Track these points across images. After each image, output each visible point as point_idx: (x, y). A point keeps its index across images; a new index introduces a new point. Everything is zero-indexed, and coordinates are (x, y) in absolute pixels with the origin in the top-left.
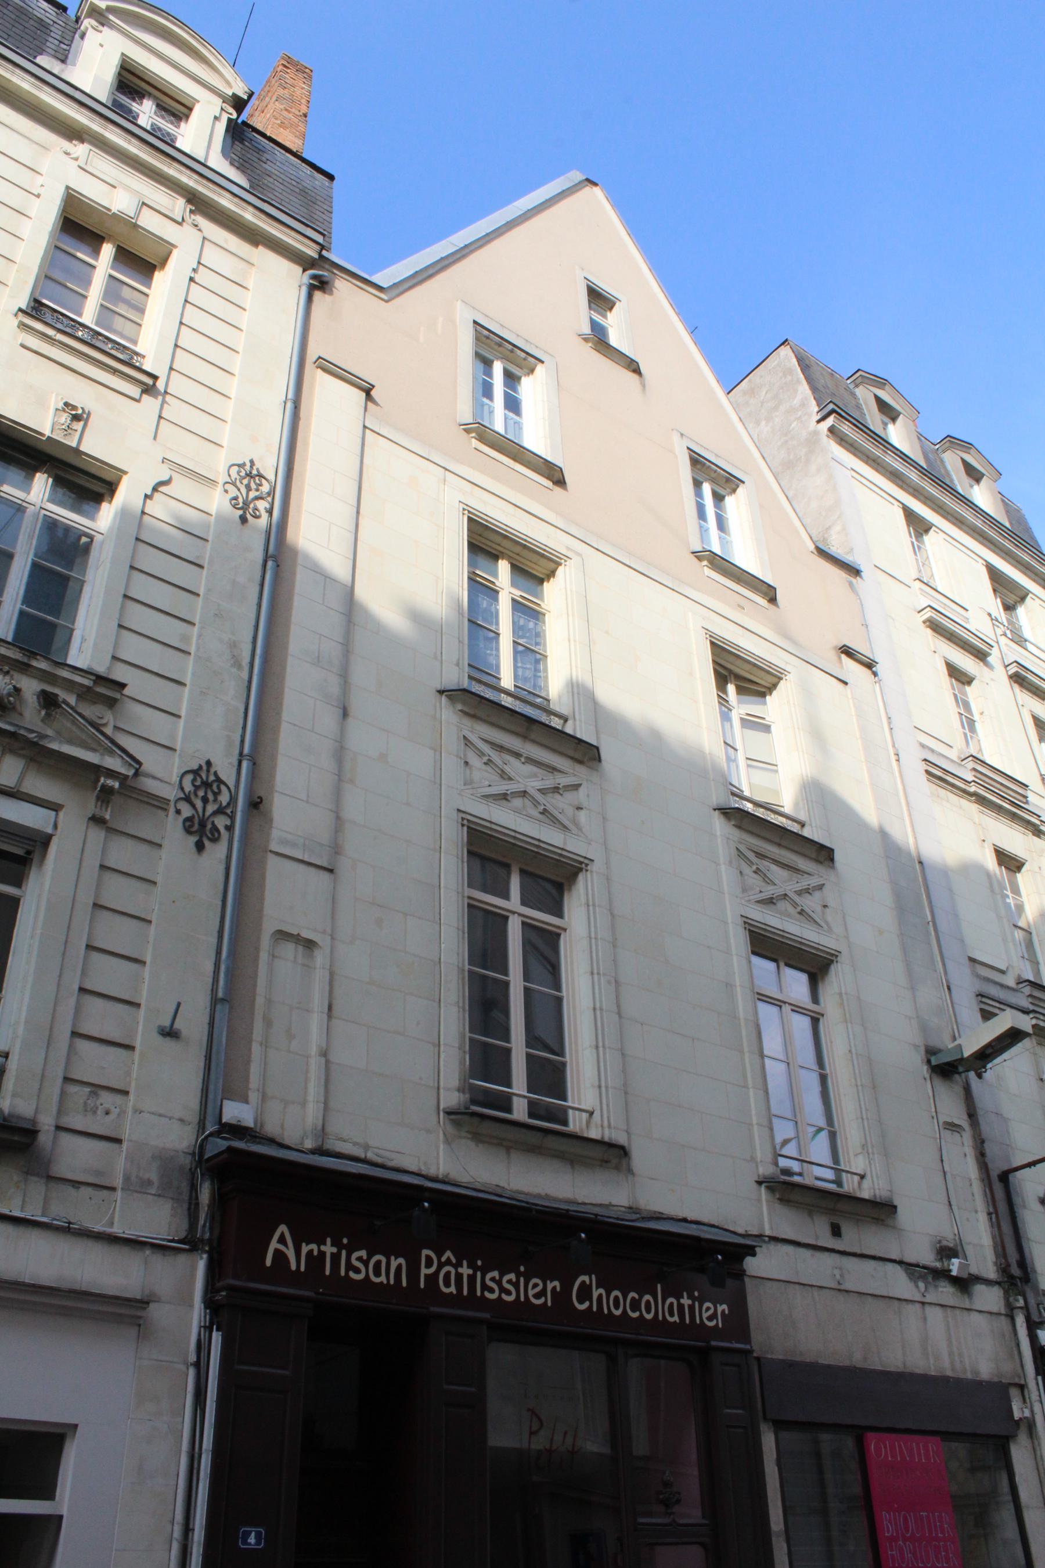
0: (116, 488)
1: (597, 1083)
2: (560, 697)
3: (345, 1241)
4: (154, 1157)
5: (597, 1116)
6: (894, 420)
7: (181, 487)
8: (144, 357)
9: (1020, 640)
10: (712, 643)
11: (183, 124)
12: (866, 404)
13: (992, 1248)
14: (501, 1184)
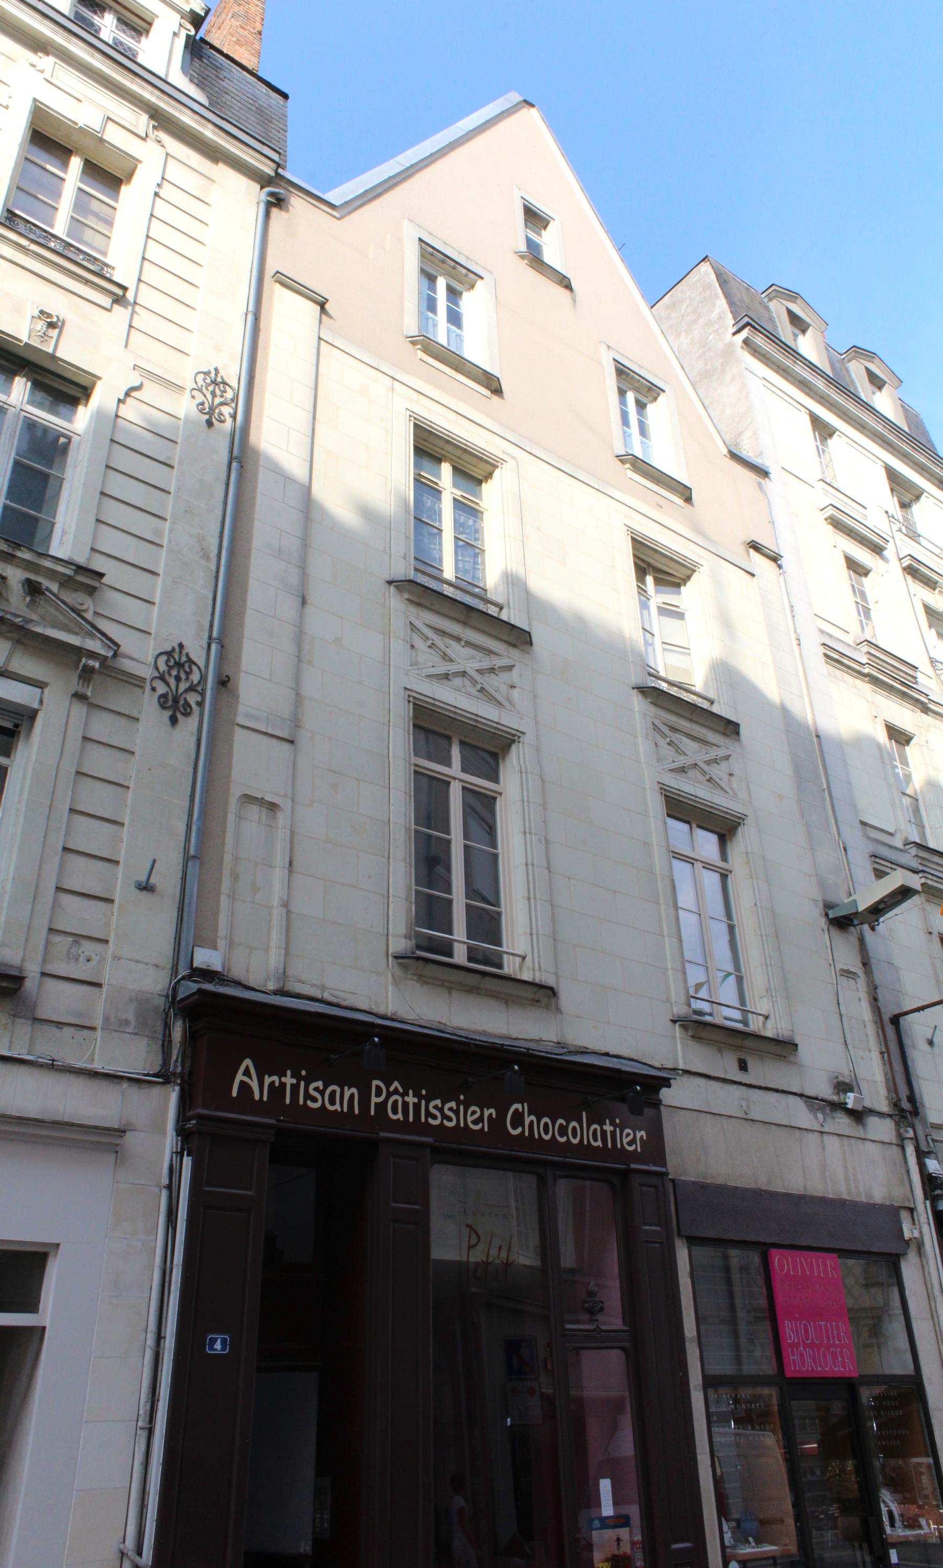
0: (91, 393)
1: (528, 931)
2: (496, 587)
4: (131, 1000)
5: (528, 960)
6: (804, 331)
7: (151, 392)
8: (113, 268)
9: (914, 536)
10: (633, 539)
11: (143, 39)
12: (779, 317)
13: (884, 1084)
14: (444, 1021)
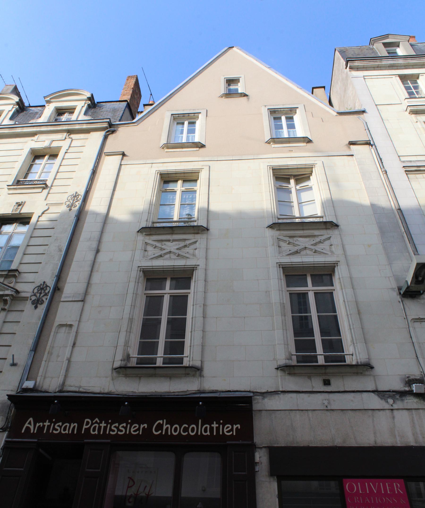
3: (221, 421)
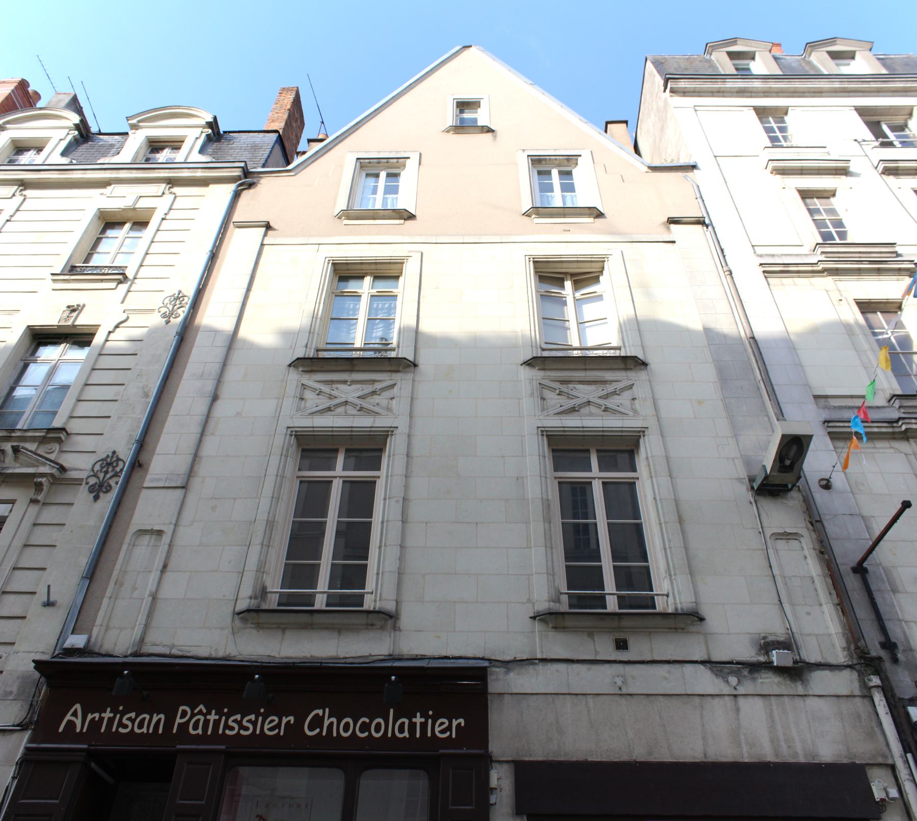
5: (671, 595)
7: (134, 320)
